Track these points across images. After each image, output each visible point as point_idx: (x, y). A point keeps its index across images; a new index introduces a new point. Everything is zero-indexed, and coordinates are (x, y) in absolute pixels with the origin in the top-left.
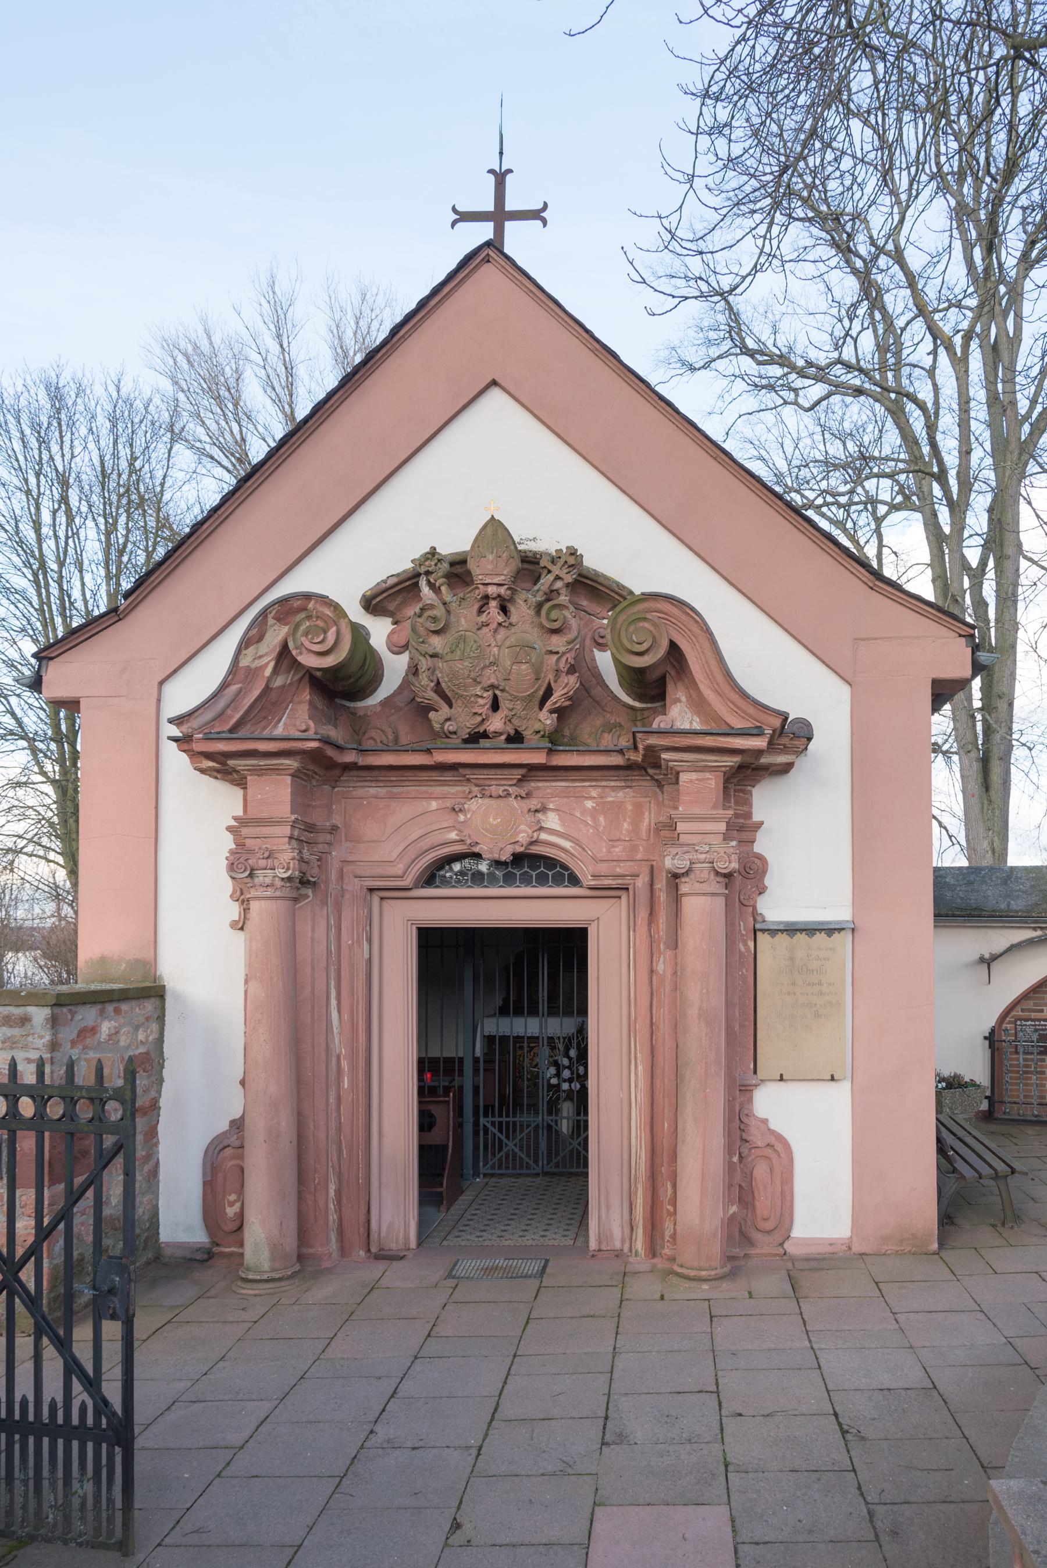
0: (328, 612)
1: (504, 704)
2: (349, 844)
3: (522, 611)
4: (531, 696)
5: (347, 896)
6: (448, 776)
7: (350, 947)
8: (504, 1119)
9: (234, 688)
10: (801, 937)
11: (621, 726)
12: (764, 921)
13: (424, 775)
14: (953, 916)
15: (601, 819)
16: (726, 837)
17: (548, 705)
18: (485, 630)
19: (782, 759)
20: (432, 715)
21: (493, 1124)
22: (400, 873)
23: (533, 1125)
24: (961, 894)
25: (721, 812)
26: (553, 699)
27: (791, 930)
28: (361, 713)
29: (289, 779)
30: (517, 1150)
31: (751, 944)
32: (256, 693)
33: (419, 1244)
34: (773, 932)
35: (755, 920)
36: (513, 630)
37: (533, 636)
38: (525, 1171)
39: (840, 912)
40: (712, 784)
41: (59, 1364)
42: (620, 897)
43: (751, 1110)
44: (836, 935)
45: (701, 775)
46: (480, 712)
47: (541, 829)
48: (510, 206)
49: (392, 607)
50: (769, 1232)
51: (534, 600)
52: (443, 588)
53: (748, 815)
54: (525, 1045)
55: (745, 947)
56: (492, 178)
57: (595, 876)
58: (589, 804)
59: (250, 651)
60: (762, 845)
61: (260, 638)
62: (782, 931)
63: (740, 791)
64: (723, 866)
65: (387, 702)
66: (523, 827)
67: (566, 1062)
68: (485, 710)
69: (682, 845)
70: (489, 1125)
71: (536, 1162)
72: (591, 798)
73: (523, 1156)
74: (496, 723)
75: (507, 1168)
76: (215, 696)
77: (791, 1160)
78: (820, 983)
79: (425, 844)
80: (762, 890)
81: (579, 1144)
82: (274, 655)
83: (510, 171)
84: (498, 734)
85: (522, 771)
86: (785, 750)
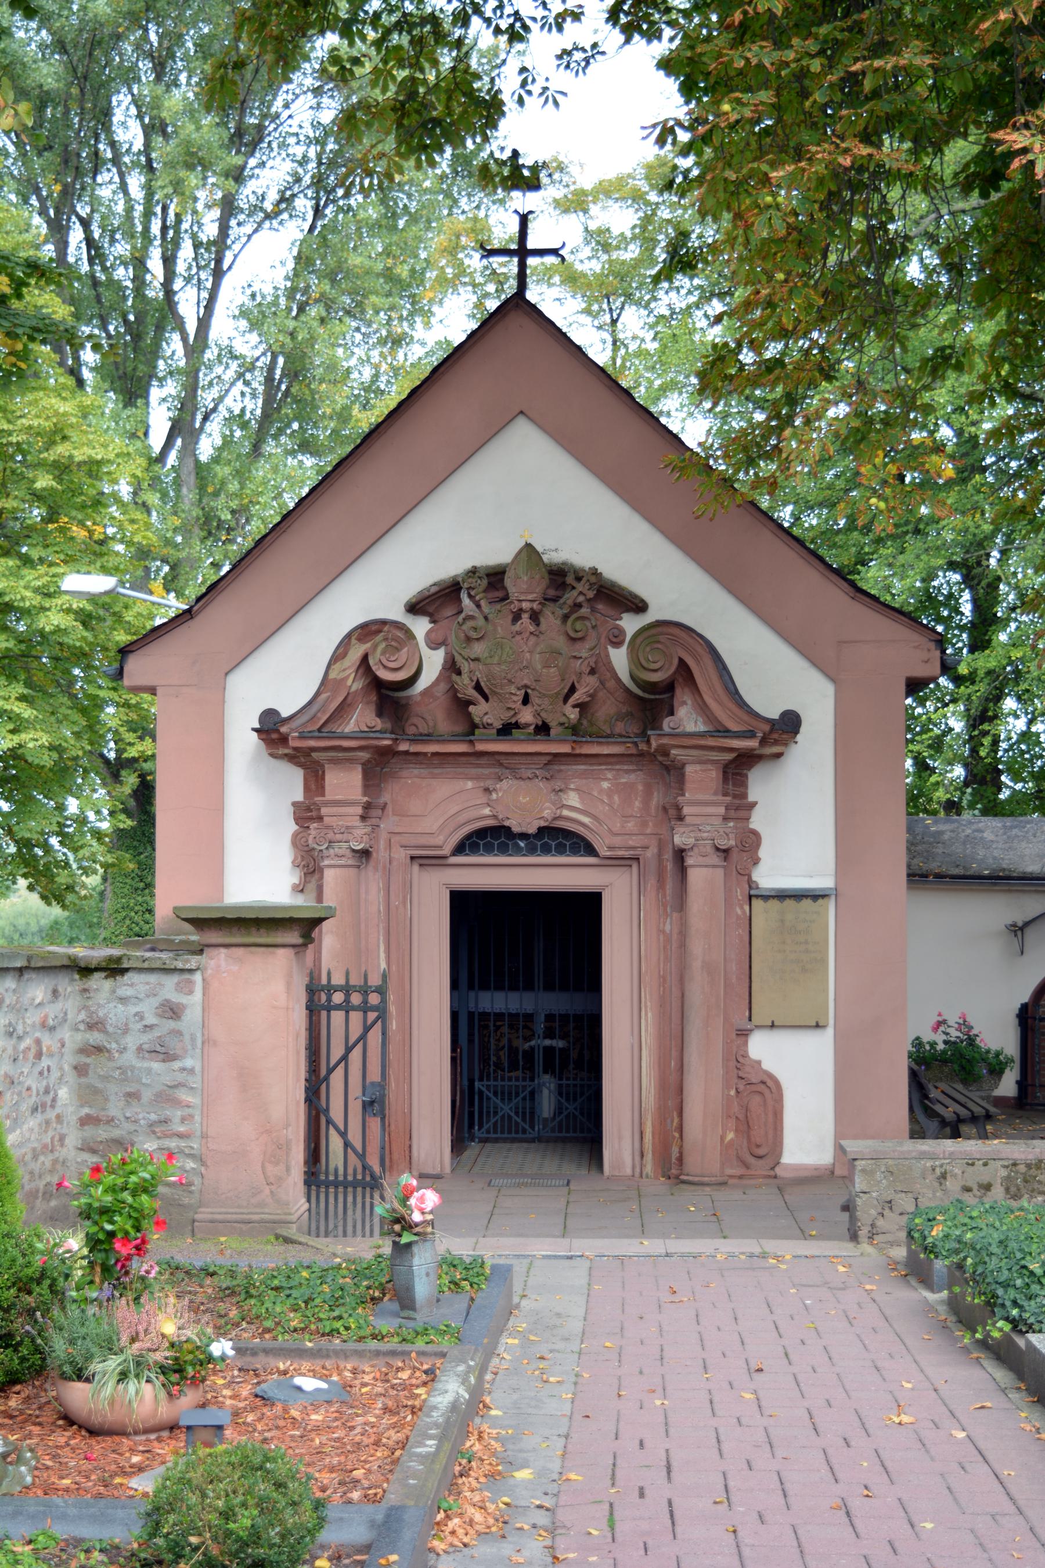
0: (400, 634)
1: (534, 698)
2: (397, 818)
3: (551, 619)
4: (557, 694)
5: (395, 863)
6: (483, 761)
7: (397, 908)
9: (324, 696)
10: (789, 903)
12: (758, 888)
13: (463, 759)
15: (616, 798)
16: (726, 819)
17: (572, 700)
18: (518, 638)
19: (775, 749)
20: (471, 708)
21: (488, 1087)
22: (440, 843)
24: (996, 853)
25: (721, 798)
26: (576, 696)
27: (782, 896)
29: (359, 768)
30: (512, 1114)
31: (747, 908)
32: (340, 699)
33: (453, 1170)
34: (766, 898)
35: (750, 887)
36: (542, 637)
37: (561, 643)
38: (520, 1135)
39: (826, 882)
40: (714, 774)
41: (350, 1136)
43: (746, 1052)
44: (820, 901)
45: (704, 767)
47: (563, 806)
48: (531, 245)
49: (431, 609)
50: (760, 1157)
51: (560, 612)
53: (744, 796)
54: (491, 1024)
57: (610, 848)
58: (605, 785)
59: (337, 667)
60: (757, 821)
61: (344, 655)
62: (773, 897)
64: (723, 843)
65: (426, 692)
66: (547, 804)
68: (518, 705)
69: (688, 825)
71: (532, 1127)
72: (606, 779)
73: (519, 1120)
74: (527, 716)
75: (502, 1132)
76: (310, 703)
78: (806, 942)
80: (756, 861)
83: (531, 212)
84: (527, 725)
85: (548, 758)
86: (776, 742)
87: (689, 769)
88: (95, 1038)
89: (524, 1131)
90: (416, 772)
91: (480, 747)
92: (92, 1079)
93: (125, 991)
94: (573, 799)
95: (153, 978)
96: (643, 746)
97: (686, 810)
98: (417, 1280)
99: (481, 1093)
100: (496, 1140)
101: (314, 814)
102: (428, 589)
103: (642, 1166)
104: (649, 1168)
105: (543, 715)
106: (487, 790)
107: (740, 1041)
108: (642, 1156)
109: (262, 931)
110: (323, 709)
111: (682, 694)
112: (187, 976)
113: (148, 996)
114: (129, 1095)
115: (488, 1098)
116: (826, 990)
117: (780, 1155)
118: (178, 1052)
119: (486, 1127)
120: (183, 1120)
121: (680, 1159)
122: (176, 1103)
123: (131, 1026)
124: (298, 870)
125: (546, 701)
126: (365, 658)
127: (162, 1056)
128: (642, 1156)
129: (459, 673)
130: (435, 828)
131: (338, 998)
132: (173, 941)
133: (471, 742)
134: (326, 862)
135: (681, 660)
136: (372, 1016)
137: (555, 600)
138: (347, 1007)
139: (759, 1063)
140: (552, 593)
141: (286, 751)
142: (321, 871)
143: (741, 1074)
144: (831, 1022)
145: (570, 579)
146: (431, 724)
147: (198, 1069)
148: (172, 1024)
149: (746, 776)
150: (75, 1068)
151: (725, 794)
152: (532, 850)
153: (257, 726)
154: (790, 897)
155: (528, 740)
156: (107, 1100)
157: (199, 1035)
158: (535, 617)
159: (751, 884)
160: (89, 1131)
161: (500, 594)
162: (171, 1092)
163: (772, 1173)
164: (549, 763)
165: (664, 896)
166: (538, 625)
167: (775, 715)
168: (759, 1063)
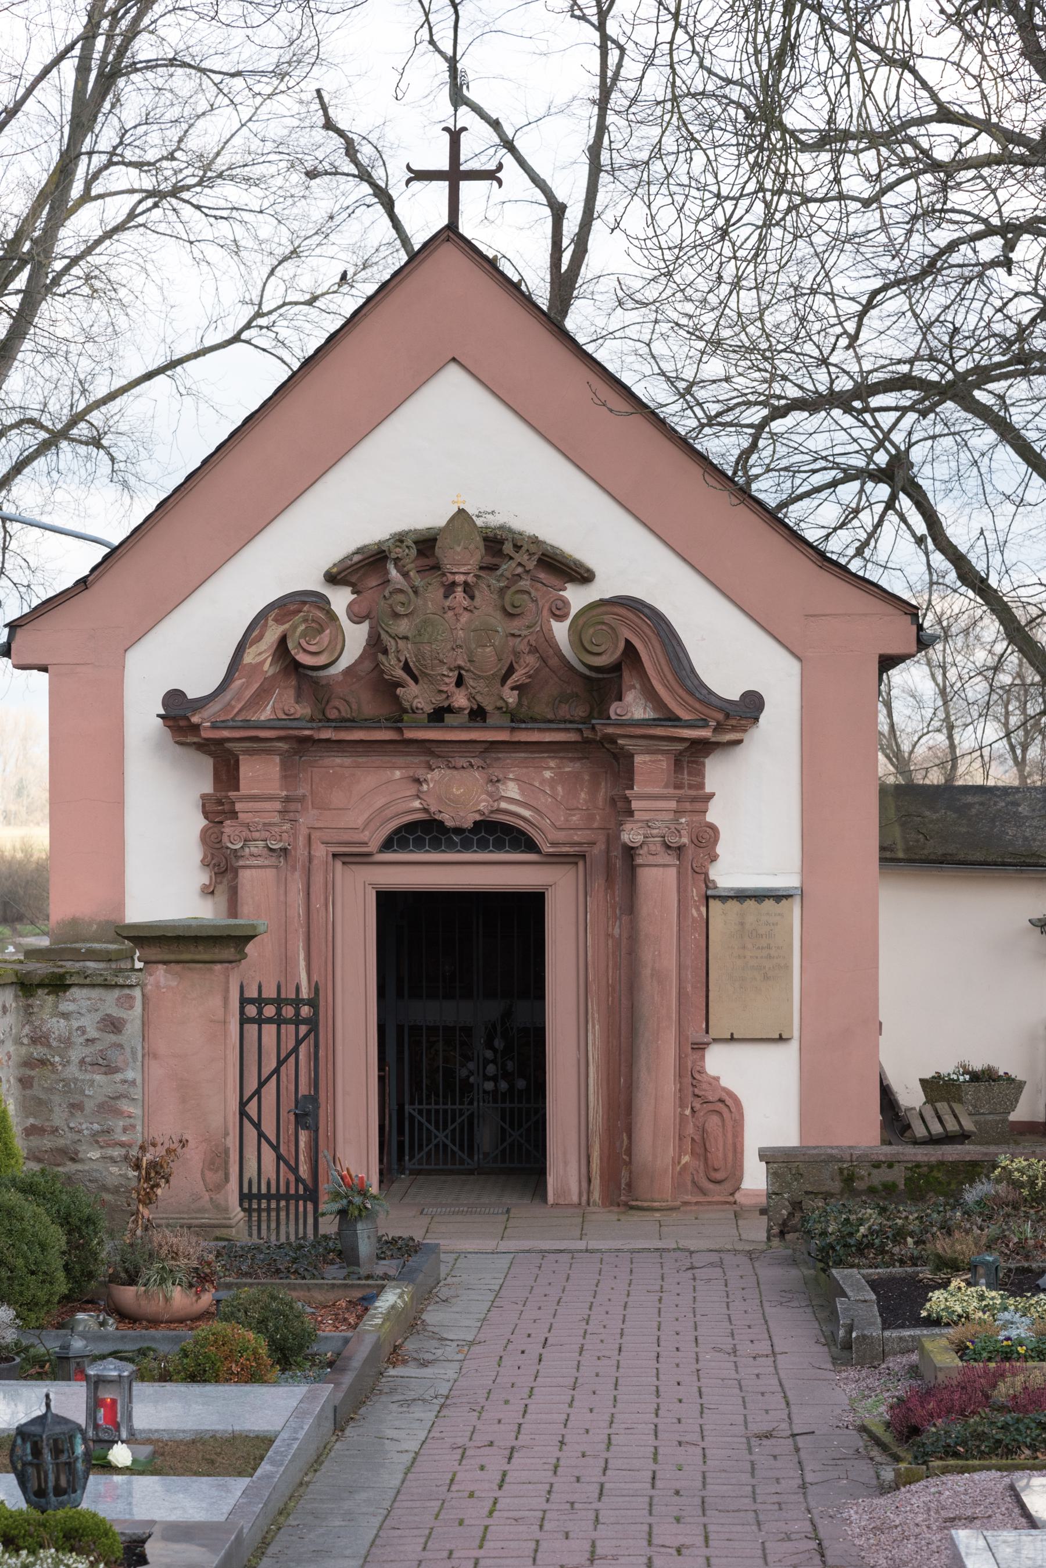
0: (321, 615)
1: (470, 681)
2: (315, 812)
3: (485, 598)
5: (315, 862)
7: (318, 910)
8: (433, 1107)
10: (751, 904)
11: (577, 696)
12: (716, 887)
13: (391, 747)
14: (1004, 864)
15: (560, 789)
17: (510, 682)
20: (399, 691)
21: (420, 1112)
22: (366, 839)
23: (467, 1114)
27: (741, 896)
28: (324, 682)
29: (277, 759)
30: (448, 1142)
31: (703, 910)
34: (723, 898)
35: (707, 887)
39: (788, 880)
40: (664, 765)
42: (576, 863)
43: (703, 1067)
44: (784, 901)
46: (445, 689)
49: (353, 579)
52: (411, 574)
53: (701, 786)
55: (696, 913)
56: (446, 137)
57: (553, 844)
58: (548, 774)
62: (732, 897)
63: (693, 762)
65: (349, 671)
66: (484, 796)
67: (489, 1054)
68: (452, 687)
70: (415, 1114)
71: (471, 1156)
73: (456, 1149)
74: (460, 700)
77: (742, 1115)
78: (769, 947)
79: (388, 813)
80: (714, 858)
81: (521, 1136)
82: (272, 651)
83: (464, 129)
84: (461, 709)
86: (734, 729)
87: (638, 759)
88: (38, 1052)
89: (462, 1162)
90: (338, 760)
91: (409, 734)
92: (36, 1091)
93: (65, 1006)
94: (512, 790)
95: (95, 993)
96: (588, 734)
97: (635, 805)
98: (360, 1241)
99: (412, 1118)
100: (429, 1172)
101: (226, 807)
102: (349, 557)
103: (589, 1192)
104: (596, 1195)
105: (479, 698)
106: (418, 781)
107: (696, 1055)
108: (589, 1181)
109: (201, 948)
110: (238, 696)
111: (628, 677)
112: (127, 991)
113: (89, 1011)
114: (72, 1106)
115: (420, 1124)
116: (790, 1000)
117: (740, 1179)
118: (120, 1065)
119: (417, 1157)
120: (125, 1130)
121: (629, 1185)
122: (118, 1113)
123: (73, 1039)
124: (207, 869)
125: (482, 683)
126: (283, 640)
127: (103, 1069)
128: (589, 1181)
129: (385, 652)
130: (360, 822)
131: (270, 1011)
132: (78, 950)
133: (400, 730)
134: (241, 863)
135: (628, 642)
136: (303, 1029)
137: (492, 568)
138: (279, 1021)
139: (717, 1079)
140: (489, 560)
141: (196, 740)
142: (235, 871)
143: (697, 1091)
144: (796, 1034)
145: (508, 548)
146: (354, 707)
147: (139, 1081)
148: (113, 1038)
149: (703, 764)
150: (20, 1080)
151: (678, 786)
152: (466, 846)
153: (162, 712)
154: (750, 897)
155: (462, 728)
156: (51, 1111)
157: (139, 1048)
158: (468, 589)
159: (708, 883)
160: (35, 1141)
161: (430, 562)
162: (113, 1102)
163: (731, 1199)
164: (486, 750)
165: (613, 896)
166: (472, 598)
167: (735, 697)
168: (717, 1079)
